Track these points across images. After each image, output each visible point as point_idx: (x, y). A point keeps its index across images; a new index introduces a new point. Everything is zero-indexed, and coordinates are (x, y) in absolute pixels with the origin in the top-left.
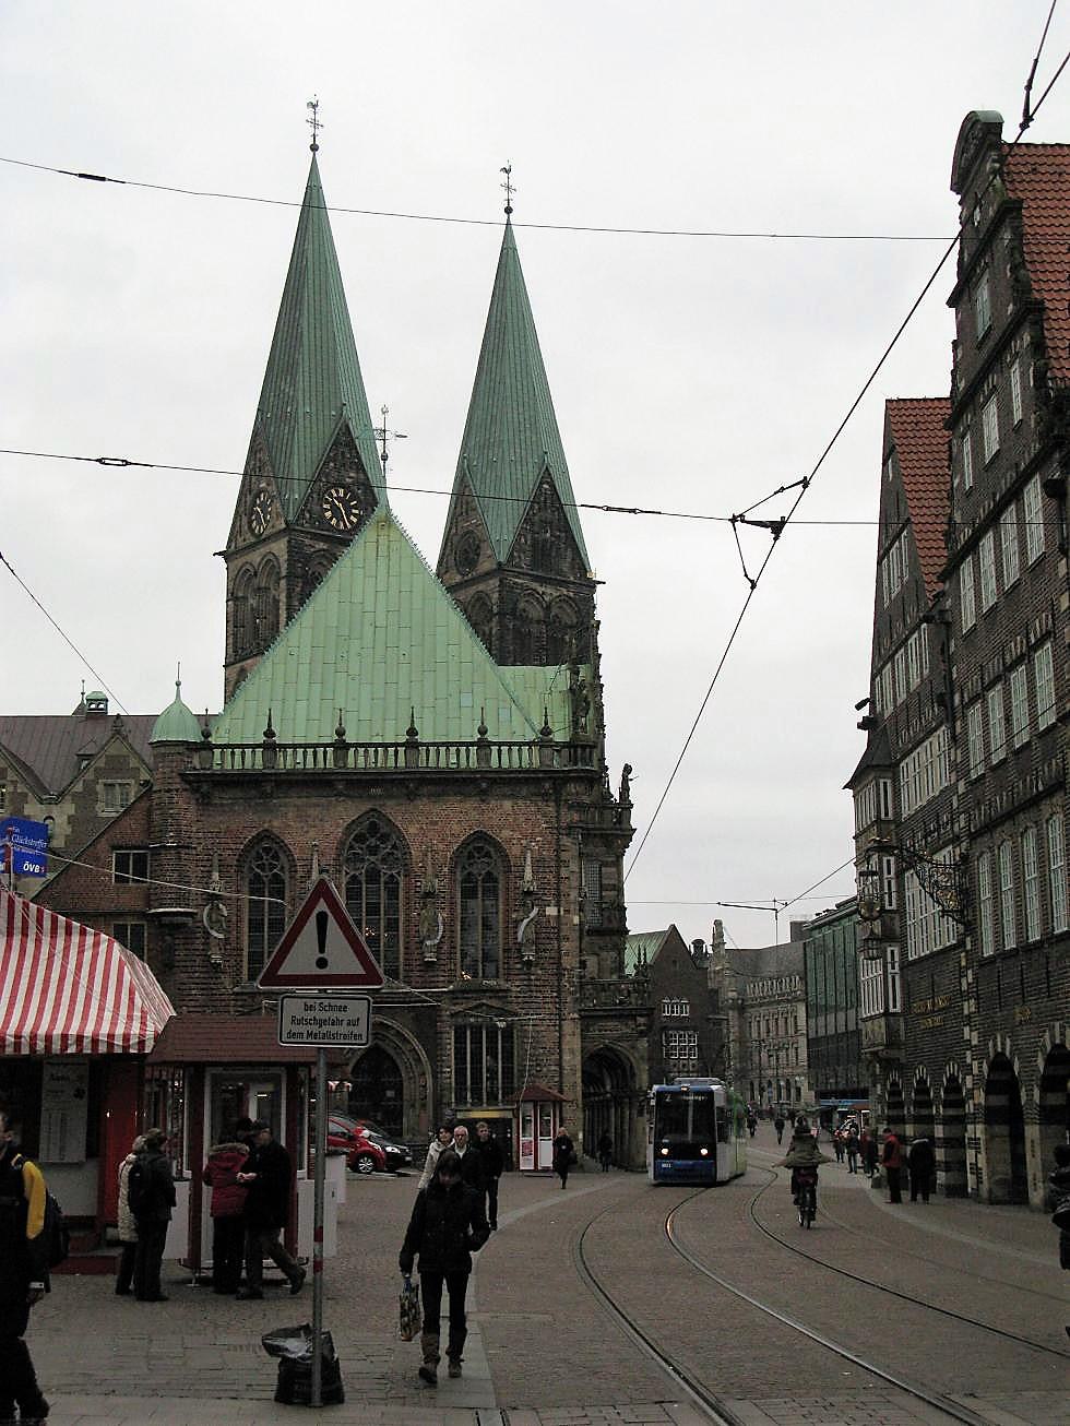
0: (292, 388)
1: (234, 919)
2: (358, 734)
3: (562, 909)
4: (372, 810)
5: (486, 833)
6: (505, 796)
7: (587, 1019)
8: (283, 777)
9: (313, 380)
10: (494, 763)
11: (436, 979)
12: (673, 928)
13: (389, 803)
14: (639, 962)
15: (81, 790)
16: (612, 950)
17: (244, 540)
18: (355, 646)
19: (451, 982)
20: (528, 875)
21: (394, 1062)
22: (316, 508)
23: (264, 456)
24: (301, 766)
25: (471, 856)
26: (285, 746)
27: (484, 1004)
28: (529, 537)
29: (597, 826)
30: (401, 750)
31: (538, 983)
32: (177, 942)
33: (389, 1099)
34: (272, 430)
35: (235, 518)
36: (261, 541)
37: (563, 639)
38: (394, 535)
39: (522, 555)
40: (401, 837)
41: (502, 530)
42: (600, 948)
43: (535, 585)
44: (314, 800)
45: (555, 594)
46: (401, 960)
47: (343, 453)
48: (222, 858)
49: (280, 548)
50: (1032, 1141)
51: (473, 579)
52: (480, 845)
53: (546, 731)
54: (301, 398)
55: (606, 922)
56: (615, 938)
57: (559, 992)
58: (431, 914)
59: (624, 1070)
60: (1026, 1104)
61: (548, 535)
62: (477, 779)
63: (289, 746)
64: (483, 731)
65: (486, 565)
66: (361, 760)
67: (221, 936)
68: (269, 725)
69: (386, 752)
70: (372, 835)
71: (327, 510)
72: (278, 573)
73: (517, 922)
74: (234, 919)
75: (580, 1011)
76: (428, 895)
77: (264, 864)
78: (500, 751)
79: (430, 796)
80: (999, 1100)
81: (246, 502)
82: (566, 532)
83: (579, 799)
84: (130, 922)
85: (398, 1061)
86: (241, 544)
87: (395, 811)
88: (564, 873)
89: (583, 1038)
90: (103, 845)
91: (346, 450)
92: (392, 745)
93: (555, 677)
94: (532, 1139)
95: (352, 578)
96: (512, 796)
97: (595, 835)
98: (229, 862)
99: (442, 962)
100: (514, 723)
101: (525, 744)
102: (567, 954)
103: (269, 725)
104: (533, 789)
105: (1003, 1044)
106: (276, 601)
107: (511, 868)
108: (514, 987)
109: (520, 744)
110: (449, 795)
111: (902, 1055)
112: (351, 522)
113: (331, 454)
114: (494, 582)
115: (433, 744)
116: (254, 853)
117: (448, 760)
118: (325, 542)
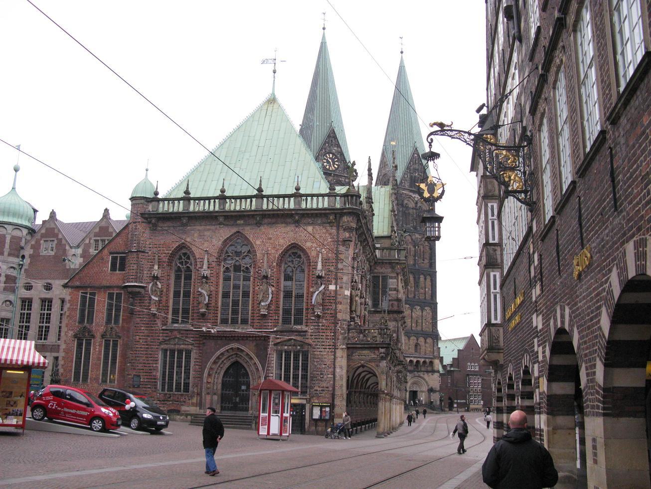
1: (165, 290)
3: (338, 287)
4: (238, 232)
5: (298, 245)
6: (309, 224)
7: (351, 349)
8: (192, 215)
9: (325, 114)
11: (267, 324)
12: (472, 335)
13: (245, 228)
15: (110, 231)
20: (319, 266)
21: (246, 370)
28: (409, 175)
29: (388, 258)
30: (254, 200)
31: (323, 328)
32: (136, 301)
33: (243, 391)
38: (276, 106)
43: (411, 194)
44: (208, 227)
48: (160, 258)
50: (594, 440)
52: (294, 251)
55: (390, 307)
57: (335, 333)
60: (586, 387)
67: (157, 299)
74: (165, 290)
75: (347, 344)
80: (564, 388)
84: (115, 292)
85: (248, 369)
87: (249, 232)
88: (340, 266)
90: (106, 251)
91: (333, 139)
94: (267, 414)
97: (386, 263)
98: (164, 259)
99: (271, 315)
104: (324, 220)
105: (563, 316)
107: (312, 265)
108: (310, 329)
110: (279, 224)
111: (501, 358)
112: (335, 167)
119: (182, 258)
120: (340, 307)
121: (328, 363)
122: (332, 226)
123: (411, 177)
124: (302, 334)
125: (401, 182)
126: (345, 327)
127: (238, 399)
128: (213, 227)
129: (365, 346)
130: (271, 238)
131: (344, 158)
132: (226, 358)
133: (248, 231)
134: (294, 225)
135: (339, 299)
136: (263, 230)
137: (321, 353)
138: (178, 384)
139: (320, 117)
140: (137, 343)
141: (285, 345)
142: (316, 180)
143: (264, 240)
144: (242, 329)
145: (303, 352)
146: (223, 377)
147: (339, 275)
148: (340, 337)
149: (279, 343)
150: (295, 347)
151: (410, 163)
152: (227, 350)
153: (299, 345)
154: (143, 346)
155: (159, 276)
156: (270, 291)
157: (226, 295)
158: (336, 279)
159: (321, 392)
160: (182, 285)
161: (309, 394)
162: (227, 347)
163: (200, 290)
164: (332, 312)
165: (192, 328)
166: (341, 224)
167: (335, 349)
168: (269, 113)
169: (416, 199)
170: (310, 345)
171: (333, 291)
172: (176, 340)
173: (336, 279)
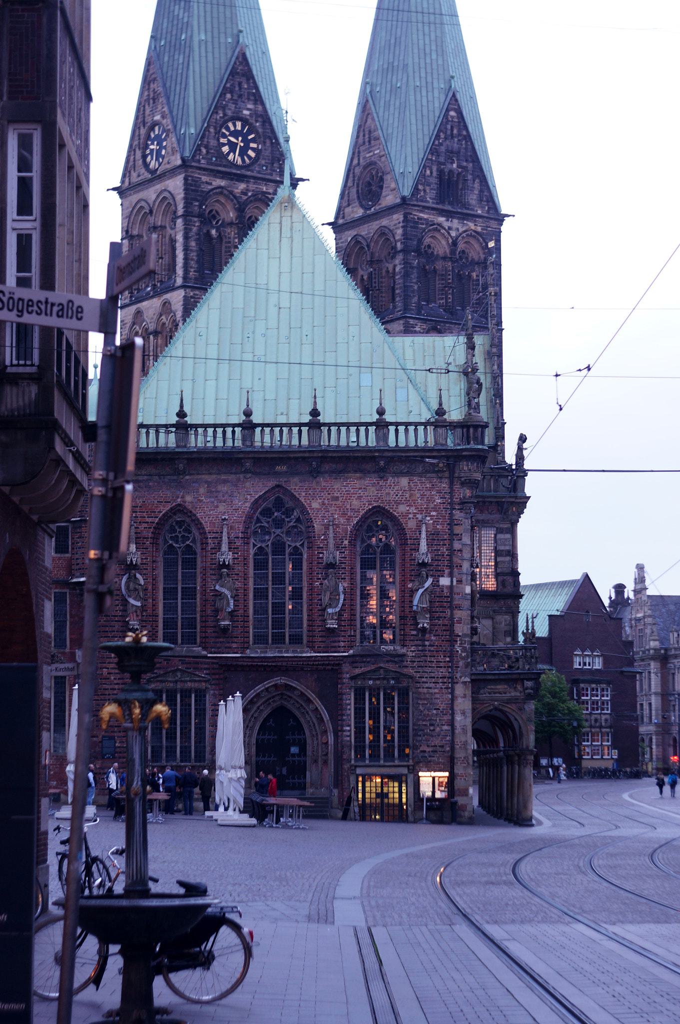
0: (186, 14)
1: (150, 587)
2: (264, 414)
4: (278, 486)
6: (402, 474)
7: (478, 683)
8: (194, 456)
10: (392, 442)
11: (336, 644)
12: (587, 577)
13: (291, 479)
14: (527, 629)
16: (506, 613)
17: (139, 176)
18: (260, 327)
19: (351, 647)
20: (423, 546)
22: (213, 143)
23: (157, 86)
24: (210, 445)
25: (369, 529)
26: (196, 426)
27: (381, 668)
28: (435, 168)
30: (305, 430)
31: (432, 649)
33: (293, 755)
34: (166, 59)
35: (129, 152)
36: (156, 177)
37: (470, 276)
39: (428, 188)
40: (304, 510)
41: (405, 162)
42: (494, 611)
43: (442, 219)
45: (461, 230)
46: (305, 626)
47: (240, 84)
49: (176, 185)
51: (374, 214)
52: (378, 517)
53: (440, 412)
54: (195, 23)
56: (509, 602)
58: (333, 583)
59: (513, 730)
61: (455, 166)
62: (374, 457)
63: (201, 426)
64: (381, 412)
65: (389, 199)
66: (267, 438)
67: (139, 604)
68: (182, 406)
69: (290, 431)
70: (277, 510)
71: (224, 145)
72: (175, 212)
73: (413, 592)
75: (472, 674)
76: (331, 566)
77: (177, 536)
78: (397, 431)
79: (332, 472)
81: (139, 135)
82: (473, 162)
83: (479, 474)
85: (302, 720)
86: (135, 179)
87: (297, 487)
89: (474, 700)
91: (243, 80)
92: (295, 425)
93: (449, 347)
95: (258, 259)
96: (409, 473)
97: (491, 502)
98: (145, 534)
100: (411, 402)
101: (421, 424)
102: (459, 622)
103: (182, 406)
106: (173, 241)
107: (408, 542)
109: (416, 425)
110: (349, 472)
113: (228, 85)
114: (398, 217)
115: (335, 424)
116: (167, 527)
117: (347, 439)
118: (222, 178)
119: (175, 531)
120: (458, 614)
121: (442, 706)
122: (441, 478)
123: (441, 173)
124: (396, 659)
125: (416, 190)
126: (467, 646)
127: (284, 771)
128: (232, 477)
129: (501, 677)
130: (338, 497)
131: (273, 131)
132: (263, 703)
133: (296, 485)
134: (376, 475)
135: (457, 600)
136: (323, 484)
137: (431, 691)
138: (185, 751)
139: (209, 19)
140: (104, 681)
141: (370, 679)
142: (399, 384)
143: (326, 502)
144: (293, 652)
145: (399, 689)
146: (258, 734)
147: (455, 559)
148: (461, 664)
149: (359, 675)
150: (385, 682)
151: (438, 137)
152: (267, 689)
153: (393, 679)
154: (116, 687)
155: (139, 563)
156: (341, 589)
157: (260, 594)
158: (451, 567)
159: (432, 754)
160: (180, 577)
161: (413, 758)
162: (268, 684)
163: (217, 587)
164: (446, 622)
165: (204, 653)
166: (456, 475)
167: (453, 683)
168: (286, 232)
169: (453, 234)
170: (411, 677)
171: (447, 587)
172: (179, 674)
173: (451, 567)
